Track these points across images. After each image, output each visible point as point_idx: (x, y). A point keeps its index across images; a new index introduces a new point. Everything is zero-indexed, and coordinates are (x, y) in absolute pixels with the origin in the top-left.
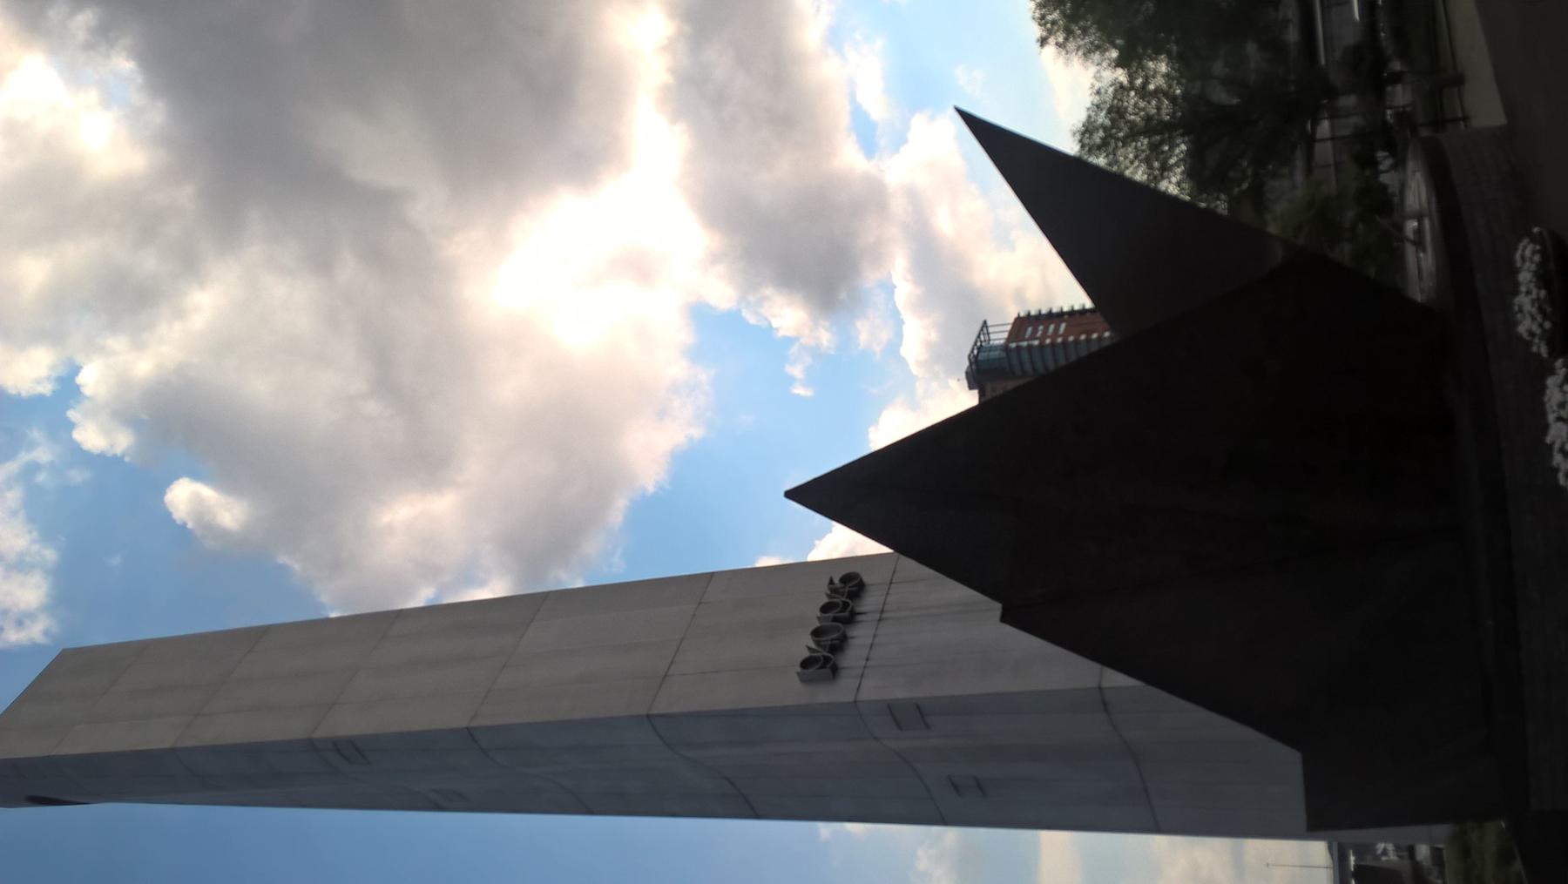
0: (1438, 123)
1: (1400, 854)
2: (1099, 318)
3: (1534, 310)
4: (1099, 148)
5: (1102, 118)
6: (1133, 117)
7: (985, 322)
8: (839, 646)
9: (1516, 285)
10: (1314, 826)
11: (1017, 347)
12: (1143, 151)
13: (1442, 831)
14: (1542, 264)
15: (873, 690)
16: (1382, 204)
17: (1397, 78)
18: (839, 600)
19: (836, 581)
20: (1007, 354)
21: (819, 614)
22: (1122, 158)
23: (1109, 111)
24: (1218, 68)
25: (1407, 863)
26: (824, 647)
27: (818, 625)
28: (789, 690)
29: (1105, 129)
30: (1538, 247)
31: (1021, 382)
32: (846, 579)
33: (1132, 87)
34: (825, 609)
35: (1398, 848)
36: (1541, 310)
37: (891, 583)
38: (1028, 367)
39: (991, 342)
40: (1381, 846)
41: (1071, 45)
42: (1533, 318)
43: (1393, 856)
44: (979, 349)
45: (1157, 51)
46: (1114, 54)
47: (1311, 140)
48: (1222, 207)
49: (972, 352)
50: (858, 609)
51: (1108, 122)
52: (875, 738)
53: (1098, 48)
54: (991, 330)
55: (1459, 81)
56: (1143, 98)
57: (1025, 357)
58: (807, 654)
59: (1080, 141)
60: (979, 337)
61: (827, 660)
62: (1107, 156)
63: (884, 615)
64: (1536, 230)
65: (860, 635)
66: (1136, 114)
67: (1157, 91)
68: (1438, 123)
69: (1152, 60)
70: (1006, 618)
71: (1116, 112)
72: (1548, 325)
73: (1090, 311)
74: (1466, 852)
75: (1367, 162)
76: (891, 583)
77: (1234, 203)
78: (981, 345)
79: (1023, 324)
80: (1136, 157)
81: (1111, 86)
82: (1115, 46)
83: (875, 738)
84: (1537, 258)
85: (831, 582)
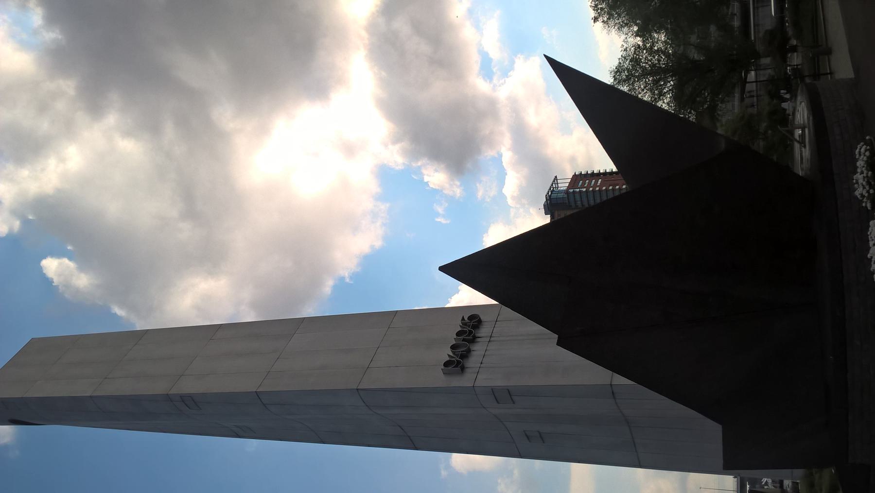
0: (816, 76)
1: (774, 485)
2: (620, 177)
4: (624, 81)
5: (627, 64)
6: (644, 65)
7: (556, 177)
8: (466, 355)
9: (856, 167)
11: (574, 191)
13: (799, 473)
15: (485, 380)
16: (782, 119)
17: (794, 49)
18: (467, 329)
19: (466, 319)
20: (568, 196)
21: (455, 337)
22: (637, 88)
24: (694, 39)
25: (778, 490)
26: (457, 355)
27: (455, 343)
28: (438, 379)
29: (628, 70)
30: (868, 147)
32: (471, 318)
34: (459, 334)
35: (773, 481)
36: (869, 183)
39: (559, 188)
41: (611, 23)
42: (864, 188)
43: (771, 486)
46: (636, 28)
47: (745, 82)
49: (548, 193)
53: (626, 24)
54: (559, 181)
55: (829, 52)
56: (650, 54)
57: (578, 197)
58: (448, 359)
59: (614, 76)
60: (552, 185)
61: (459, 362)
63: (492, 339)
65: (478, 349)
66: (646, 63)
71: (635, 61)
72: (872, 191)
73: (615, 173)
75: (775, 95)
77: (699, 115)
79: (577, 178)
80: (645, 87)
82: (636, 24)
84: (867, 153)
85: (463, 319)
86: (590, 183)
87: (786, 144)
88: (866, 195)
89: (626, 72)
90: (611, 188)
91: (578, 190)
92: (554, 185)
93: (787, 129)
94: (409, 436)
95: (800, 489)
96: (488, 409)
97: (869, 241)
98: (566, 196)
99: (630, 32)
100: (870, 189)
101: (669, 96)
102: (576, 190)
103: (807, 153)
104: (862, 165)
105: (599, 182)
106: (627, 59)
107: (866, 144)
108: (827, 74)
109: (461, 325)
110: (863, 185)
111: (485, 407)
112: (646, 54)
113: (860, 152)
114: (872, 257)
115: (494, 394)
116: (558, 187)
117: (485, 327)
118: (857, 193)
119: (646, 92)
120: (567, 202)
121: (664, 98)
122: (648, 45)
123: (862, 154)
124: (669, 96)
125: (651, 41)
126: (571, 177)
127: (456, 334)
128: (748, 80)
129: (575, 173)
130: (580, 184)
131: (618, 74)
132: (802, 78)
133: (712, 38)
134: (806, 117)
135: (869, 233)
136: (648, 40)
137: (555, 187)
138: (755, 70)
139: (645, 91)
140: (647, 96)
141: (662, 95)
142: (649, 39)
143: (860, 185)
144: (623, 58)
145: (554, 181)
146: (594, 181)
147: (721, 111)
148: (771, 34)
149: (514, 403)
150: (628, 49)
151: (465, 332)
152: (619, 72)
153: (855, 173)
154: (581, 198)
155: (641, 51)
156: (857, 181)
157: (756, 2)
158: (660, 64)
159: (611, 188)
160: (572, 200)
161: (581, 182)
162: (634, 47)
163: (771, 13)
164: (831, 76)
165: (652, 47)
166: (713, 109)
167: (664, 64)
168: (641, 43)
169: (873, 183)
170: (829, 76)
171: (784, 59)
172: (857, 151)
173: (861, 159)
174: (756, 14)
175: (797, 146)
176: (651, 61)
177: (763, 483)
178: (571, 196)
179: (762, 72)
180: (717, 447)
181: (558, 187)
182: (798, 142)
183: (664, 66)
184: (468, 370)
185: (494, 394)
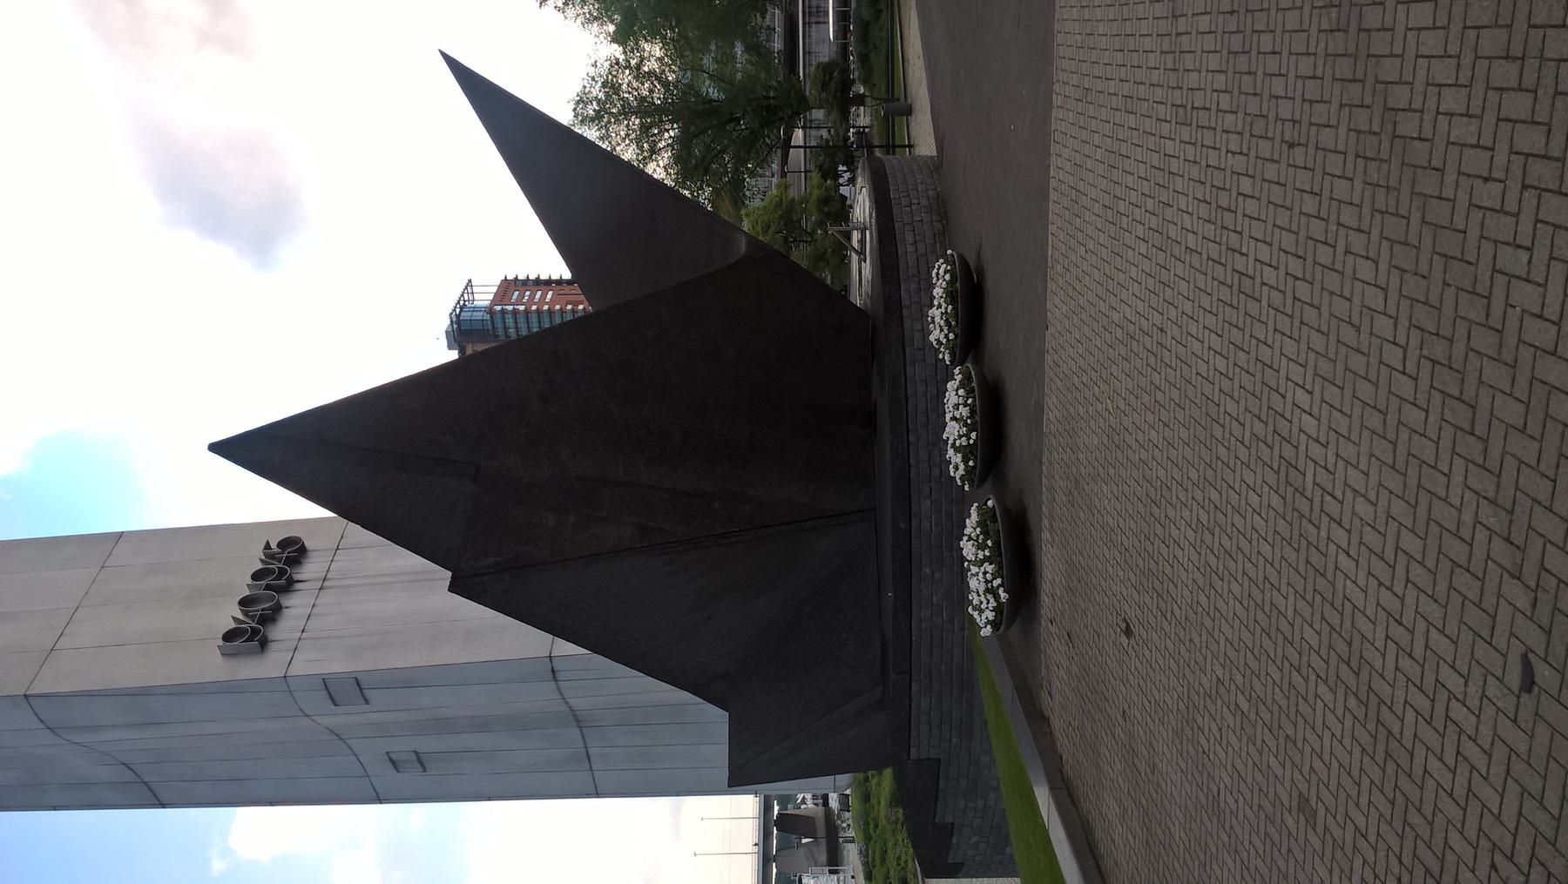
0: (890, 147)
1: (815, 801)
2: (576, 288)
3: (942, 323)
4: (592, 120)
5: (597, 91)
6: (626, 95)
7: (470, 281)
8: (272, 615)
9: (932, 298)
10: (738, 781)
11: (514, 308)
12: (634, 131)
13: (843, 779)
14: (951, 283)
15: (308, 664)
16: (839, 210)
17: (860, 101)
18: (275, 566)
19: (274, 545)
20: (492, 317)
21: (250, 581)
22: (613, 135)
23: (604, 85)
24: (707, 62)
25: (821, 808)
26: (252, 618)
27: (248, 593)
28: (212, 666)
29: (599, 101)
30: (949, 268)
31: (499, 344)
32: (284, 544)
33: (628, 66)
34: (257, 576)
35: (815, 797)
36: (948, 322)
37: (338, 549)
38: (500, 332)
39: (475, 302)
40: (800, 797)
41: (570, 12)
42: (942, 330)
43: (810, 804)
44: (461, 308)
45: (653, 35)
46: (611, 28)
47: (787, 145)
48: (705, 197)
49: (455, 310)
50: (296, 577)
51: (601, 96)
52: (306, 715)
53: (596, 18)
54: (475, 289)
55: (908, 111)
56: (636, 78)
57: (510, 321)
58: (233, 625)
59: (575, 110)
60: (462, 295)
61: (255, 632)
62: (599, 129)
63: (326, 583)
64: (949, 252)
65: (296, 605)
66: (629, 93)
67: (650, 73)
68: (890, 147)
69: (647, 41)
70: (454, 588)
71: (611, 87)
72: (951, 336)
73: (569, 282)
74: (866, 798)
75: (830, 173)
76: (338, 549)
77: (716, 198)
78: (464, 304)
79: (509, 286)
80: (628, 135)
81: (606, 61)
82: (612, 21)
83: (306, 715)
84: (947, 277)
85: (268, 546)
86: (532, 296)
87: (840, 252)
88: (944, 341)
89: (594, 103)
90: (569, 307)
91: (510, 308)
92: (466, 295)
94: (144, 782)
96: (313, 718)
97: (945, 413)
98: (488, 317)
99: (602, 33)
100: (949, 332)
101: (666, 155)
102: (507, 307)
103: (867, 269)
104: (940, 294)
105: (549, 296)
106: (596, 82)
107: (946, 262)
108: (906, 146)
109: (264, 558)
110: (940, 326)
111: (309, 714)
112: (630, 77)
113: (938, 274)
114: (948, 438)
115: (327, 689)
116: (474, 300)
117: (314, 560)
118: (932, 338)
119: (629, 144)
121: (659, 158)
122: (633, 62)
123: (940, 277)
124: (666, 155)
125: (638, 54)
126: (498, 284)
127: (252, 575)
128: (792, 144)
129: (528, 277)
130: (515, 297)
131: (580, 106)
132: (870, 147)
133: (738, 65)
134: (867, 212)
135: (945, 401)
136: (633, 53)
137: (469, 301)
138: (804, 128)
139: (627, 142)
140: (630, 151)
141: (655, 153)
142: (636, 51)
143: (937, 326)
144: (590, 79)
145: (466, 288)
146: (539, 293)
147: (748, 190)
148: (826, 69)
149: (367, 702)
150: (599, 65)
151: (270, 572)
152: (583, 102)
153: (932, 306)
155: (620, 71)
156: (933, 318)
157: (807, 15)
158: (652, 98)
159: (569, 307)
160: (500, 325)
161: (517, 293)
162: (609, 62)
164: (909, 150)
165: (639, 67)
166: (737, 186)
167: (659, 98)
168: (622, 57)
169: (953, 323)
170: (907, 149)
171: (845, 114)
172: (935, 271)
173: (939, 284)
174: (807, 34)
175: (855, 257)
176: (637, 90)
177: (799, 801)
178: (498, 318)
179: (814, 132)
180: (718, 753)
181: (474, 300)
182: (856, 251)
183: (659, 102)
184: (272, 646)
185: (327, 689)
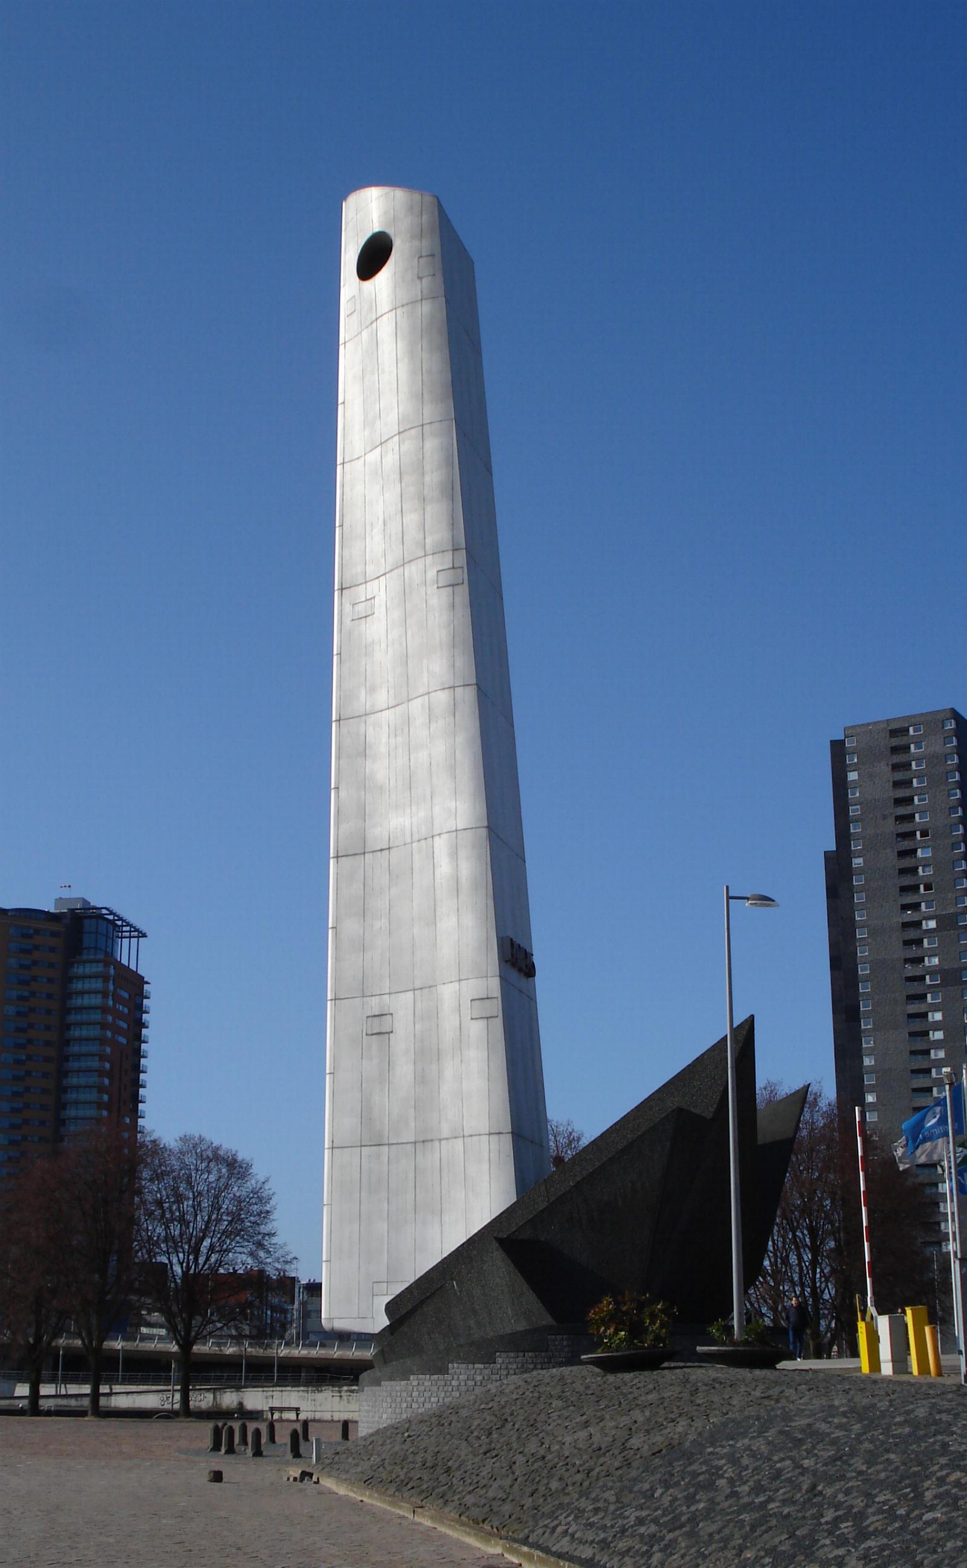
7: (144, 935)
44: (112, 922)
54: (134, 941)
60: (128, 925)
92: (128, 928)
93: (875, 1314)
95: (783, 1365)
120: (85, 957)
126: (139, 972)
129: (147, 983)
146: (124, 1025)
154: (90, 977)
161: (126, 995)
163: (873, 1283)
181: (122, 938)
